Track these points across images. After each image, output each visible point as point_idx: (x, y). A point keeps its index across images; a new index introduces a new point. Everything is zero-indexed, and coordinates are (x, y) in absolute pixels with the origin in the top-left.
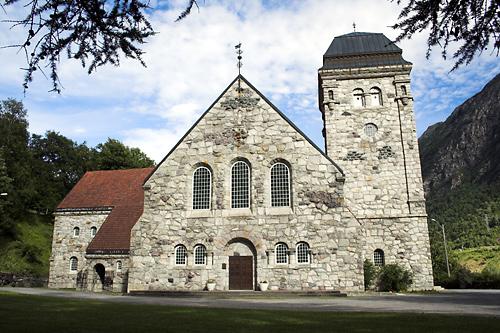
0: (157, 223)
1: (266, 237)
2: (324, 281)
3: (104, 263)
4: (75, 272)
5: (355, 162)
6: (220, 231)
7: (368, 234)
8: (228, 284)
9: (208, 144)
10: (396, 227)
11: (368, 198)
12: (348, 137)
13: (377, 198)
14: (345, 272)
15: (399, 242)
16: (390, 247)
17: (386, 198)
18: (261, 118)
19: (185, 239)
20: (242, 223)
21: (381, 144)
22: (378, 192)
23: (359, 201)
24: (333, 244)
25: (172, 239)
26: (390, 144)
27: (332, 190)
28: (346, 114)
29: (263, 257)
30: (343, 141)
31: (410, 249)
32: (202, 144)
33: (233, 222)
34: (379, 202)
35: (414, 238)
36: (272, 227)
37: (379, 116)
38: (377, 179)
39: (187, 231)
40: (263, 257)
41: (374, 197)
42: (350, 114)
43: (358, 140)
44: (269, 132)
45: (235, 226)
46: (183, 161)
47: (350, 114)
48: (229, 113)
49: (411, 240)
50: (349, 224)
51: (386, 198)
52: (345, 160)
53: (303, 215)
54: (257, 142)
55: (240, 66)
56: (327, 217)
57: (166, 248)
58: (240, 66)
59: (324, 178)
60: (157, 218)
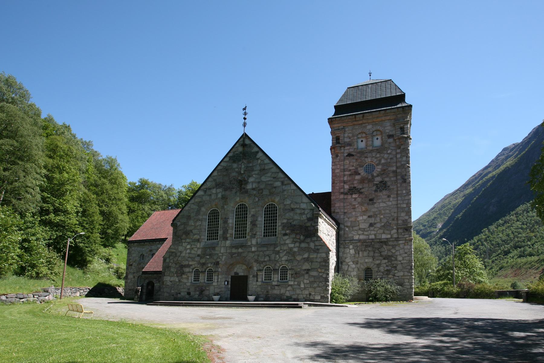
0: (181, 252)
1: (257, 261)
2: (298, 295)
3: (154, 281)
4: (430, 285)
5: (354, 196)
6: (224, 257)
7: (361, 255)
8: (229, 296)
9: (218, 190)
10: (385, 250)
11: (362, 226)
12: (350, 175)
13: (371, 225)
14: (315, 288)
15: (386, 261)
16: (379, 265)
17: (378, 225)
18: (258, 168)
19: (199, 263)
20: (240, 250)
21: (378, 179)
22: (372, 220)
23: (355, 228)
24: (306, 266)
25: (190, 263)
26: (386, 179)
27: (309, 224)
28: (350, 155)
29: (254, 276)
30: (345, 179)
31: (396, 267)
32: (214, 191)
33: (234, 251)
34: (372, 228)
35: (400, 258)
36: (261, 253)
37: (378, 155)
38: (373, 209)
39: (201, 258)
40: (254, 276)
41: (367, 225)
42: (353, 155)
43: (358, 177)
44: (264, 179)
45: (235, 253)
46: (200, 205)
47: (353, 155)
48: (235, 165)
49: (396, 260)
50: (320, 251)
51: (378, 225)
52: (346, 194)
53: (285, 244)
54: (254, 186)
55: (245, 125)
56: (303, 245)
57: (187, 270)
58: (245, 125)
59: (304, 213)
60: (180, 248)
